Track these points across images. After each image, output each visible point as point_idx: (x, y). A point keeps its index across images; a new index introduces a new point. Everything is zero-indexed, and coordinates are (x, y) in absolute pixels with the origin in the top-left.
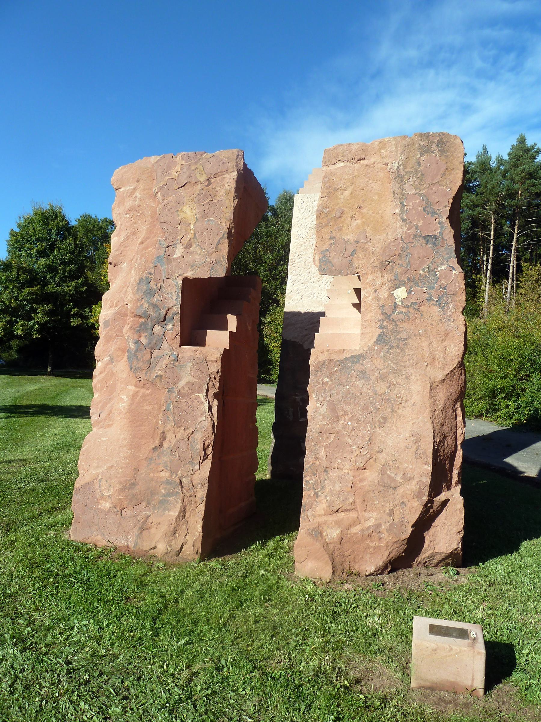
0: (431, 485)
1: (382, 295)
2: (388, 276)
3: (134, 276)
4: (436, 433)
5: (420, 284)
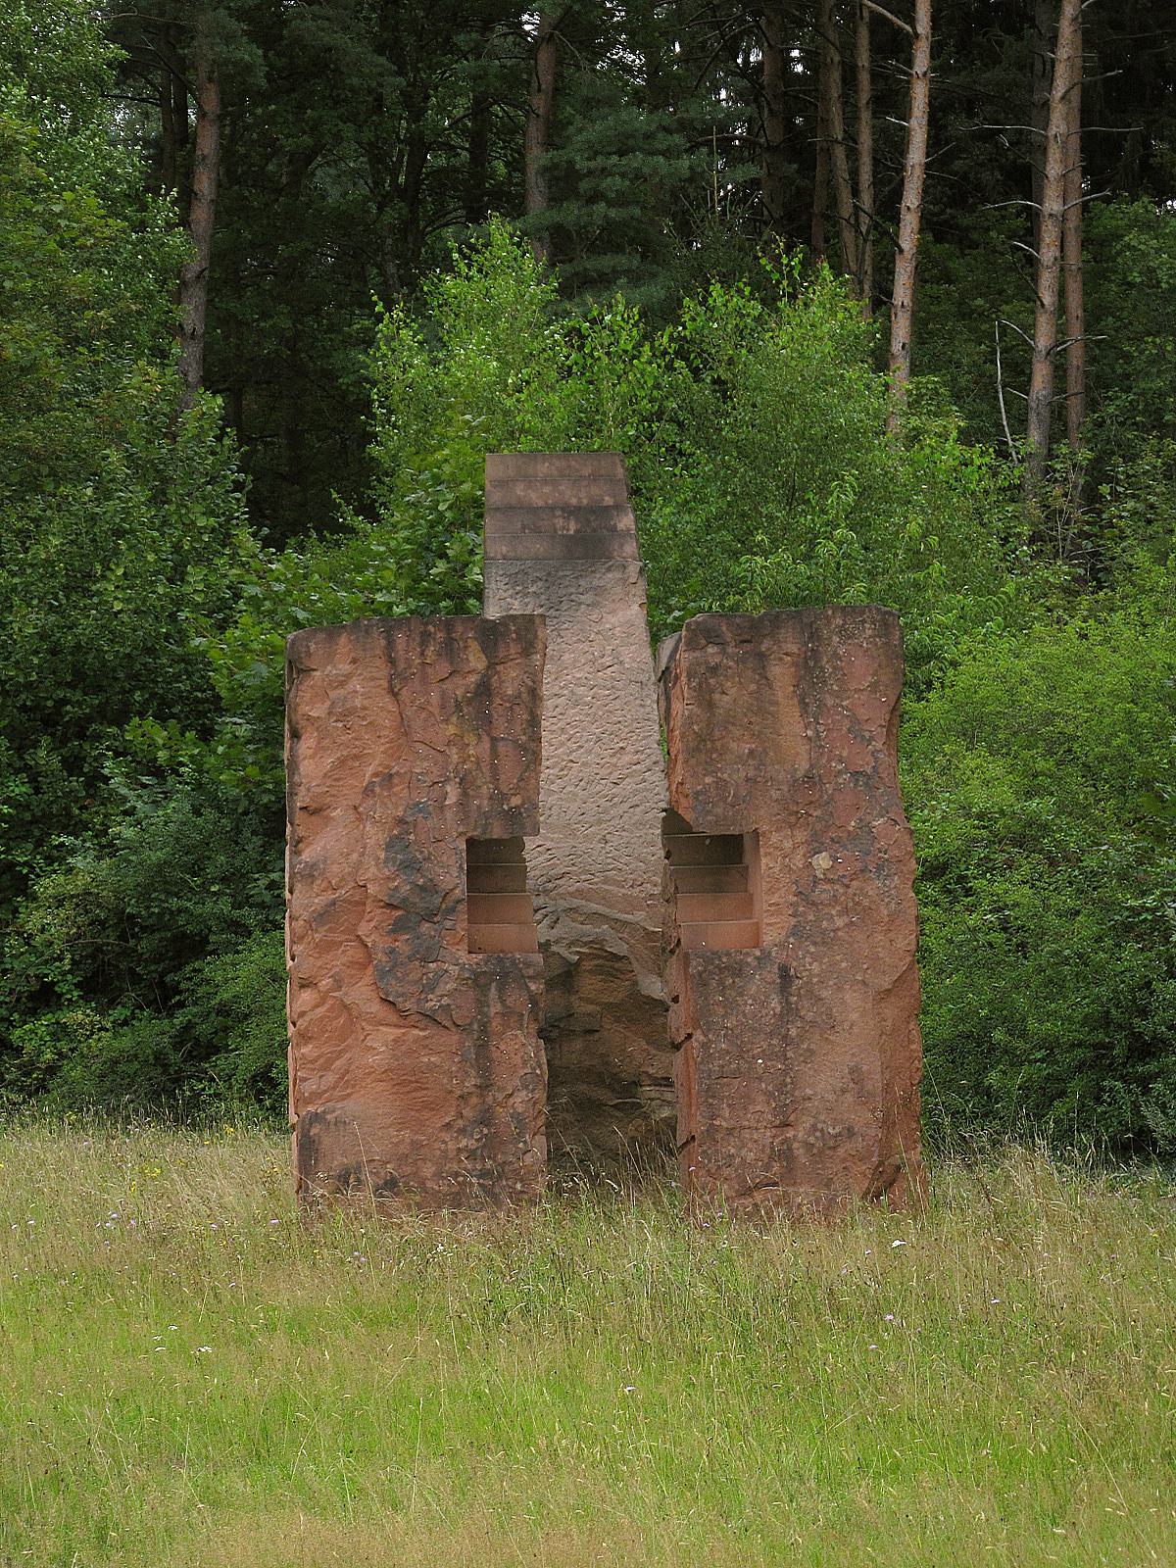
2: (801, 836)
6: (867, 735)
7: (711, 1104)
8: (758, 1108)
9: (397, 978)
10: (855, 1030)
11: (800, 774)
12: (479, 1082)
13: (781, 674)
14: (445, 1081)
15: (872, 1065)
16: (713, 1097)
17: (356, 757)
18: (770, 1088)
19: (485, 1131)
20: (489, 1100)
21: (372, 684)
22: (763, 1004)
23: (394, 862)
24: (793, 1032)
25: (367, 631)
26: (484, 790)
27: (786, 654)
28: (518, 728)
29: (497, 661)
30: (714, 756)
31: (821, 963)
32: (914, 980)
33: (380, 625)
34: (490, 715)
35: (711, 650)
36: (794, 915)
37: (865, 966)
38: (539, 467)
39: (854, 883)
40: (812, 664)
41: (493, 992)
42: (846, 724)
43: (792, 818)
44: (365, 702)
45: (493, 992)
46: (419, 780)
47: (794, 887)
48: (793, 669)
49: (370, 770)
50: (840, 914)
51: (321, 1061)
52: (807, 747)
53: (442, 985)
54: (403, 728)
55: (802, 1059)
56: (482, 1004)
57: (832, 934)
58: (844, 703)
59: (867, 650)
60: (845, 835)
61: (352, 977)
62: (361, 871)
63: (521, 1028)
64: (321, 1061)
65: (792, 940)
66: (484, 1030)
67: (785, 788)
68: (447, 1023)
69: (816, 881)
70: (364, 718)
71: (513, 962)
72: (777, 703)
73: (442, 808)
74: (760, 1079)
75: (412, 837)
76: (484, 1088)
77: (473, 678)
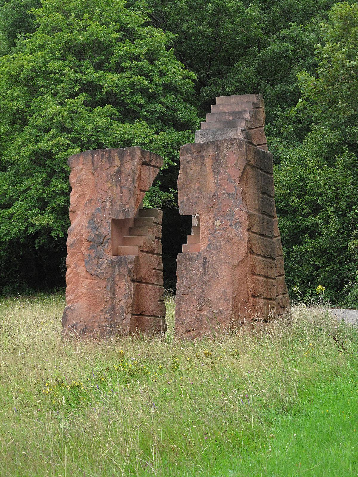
0: (65, 253)
1: (209, 224)
2: (211, 215)
3: (86, 219)
4: (234, 291)
5: (226, 218)
6: (233, 181)
10: (225, 278)
11: (212, 195)
13: (208, 161)
15: (230, 290)
17: (83, 194)
18: (197, 298)
19: (112, 312)
20: (114, 302)
21: (88, 171)
22: (198, 270)
24: (206, 279)
26: (118, 203)
28: (129, 183)
32: (248, 261)
33: (91, 153)
34: (121, 179)
35: (188, 155)
36: (209, 241)
39: (228, 230)
41: (117, 268)
42: (227, 177)
43: (210, 210)
45: (117, 268)
46: (98, 201)
48: (211, 160)
53: (102, 266)
54: (96, 185)
56: (113, 271)
63: (125, 279)
66: (113, 280)
67: (207, 199)
69: (216, 230)
71: (124, 259)
72: (206, 172)
74: (195, 295)
76: (113, 298)
77: (116, 168)
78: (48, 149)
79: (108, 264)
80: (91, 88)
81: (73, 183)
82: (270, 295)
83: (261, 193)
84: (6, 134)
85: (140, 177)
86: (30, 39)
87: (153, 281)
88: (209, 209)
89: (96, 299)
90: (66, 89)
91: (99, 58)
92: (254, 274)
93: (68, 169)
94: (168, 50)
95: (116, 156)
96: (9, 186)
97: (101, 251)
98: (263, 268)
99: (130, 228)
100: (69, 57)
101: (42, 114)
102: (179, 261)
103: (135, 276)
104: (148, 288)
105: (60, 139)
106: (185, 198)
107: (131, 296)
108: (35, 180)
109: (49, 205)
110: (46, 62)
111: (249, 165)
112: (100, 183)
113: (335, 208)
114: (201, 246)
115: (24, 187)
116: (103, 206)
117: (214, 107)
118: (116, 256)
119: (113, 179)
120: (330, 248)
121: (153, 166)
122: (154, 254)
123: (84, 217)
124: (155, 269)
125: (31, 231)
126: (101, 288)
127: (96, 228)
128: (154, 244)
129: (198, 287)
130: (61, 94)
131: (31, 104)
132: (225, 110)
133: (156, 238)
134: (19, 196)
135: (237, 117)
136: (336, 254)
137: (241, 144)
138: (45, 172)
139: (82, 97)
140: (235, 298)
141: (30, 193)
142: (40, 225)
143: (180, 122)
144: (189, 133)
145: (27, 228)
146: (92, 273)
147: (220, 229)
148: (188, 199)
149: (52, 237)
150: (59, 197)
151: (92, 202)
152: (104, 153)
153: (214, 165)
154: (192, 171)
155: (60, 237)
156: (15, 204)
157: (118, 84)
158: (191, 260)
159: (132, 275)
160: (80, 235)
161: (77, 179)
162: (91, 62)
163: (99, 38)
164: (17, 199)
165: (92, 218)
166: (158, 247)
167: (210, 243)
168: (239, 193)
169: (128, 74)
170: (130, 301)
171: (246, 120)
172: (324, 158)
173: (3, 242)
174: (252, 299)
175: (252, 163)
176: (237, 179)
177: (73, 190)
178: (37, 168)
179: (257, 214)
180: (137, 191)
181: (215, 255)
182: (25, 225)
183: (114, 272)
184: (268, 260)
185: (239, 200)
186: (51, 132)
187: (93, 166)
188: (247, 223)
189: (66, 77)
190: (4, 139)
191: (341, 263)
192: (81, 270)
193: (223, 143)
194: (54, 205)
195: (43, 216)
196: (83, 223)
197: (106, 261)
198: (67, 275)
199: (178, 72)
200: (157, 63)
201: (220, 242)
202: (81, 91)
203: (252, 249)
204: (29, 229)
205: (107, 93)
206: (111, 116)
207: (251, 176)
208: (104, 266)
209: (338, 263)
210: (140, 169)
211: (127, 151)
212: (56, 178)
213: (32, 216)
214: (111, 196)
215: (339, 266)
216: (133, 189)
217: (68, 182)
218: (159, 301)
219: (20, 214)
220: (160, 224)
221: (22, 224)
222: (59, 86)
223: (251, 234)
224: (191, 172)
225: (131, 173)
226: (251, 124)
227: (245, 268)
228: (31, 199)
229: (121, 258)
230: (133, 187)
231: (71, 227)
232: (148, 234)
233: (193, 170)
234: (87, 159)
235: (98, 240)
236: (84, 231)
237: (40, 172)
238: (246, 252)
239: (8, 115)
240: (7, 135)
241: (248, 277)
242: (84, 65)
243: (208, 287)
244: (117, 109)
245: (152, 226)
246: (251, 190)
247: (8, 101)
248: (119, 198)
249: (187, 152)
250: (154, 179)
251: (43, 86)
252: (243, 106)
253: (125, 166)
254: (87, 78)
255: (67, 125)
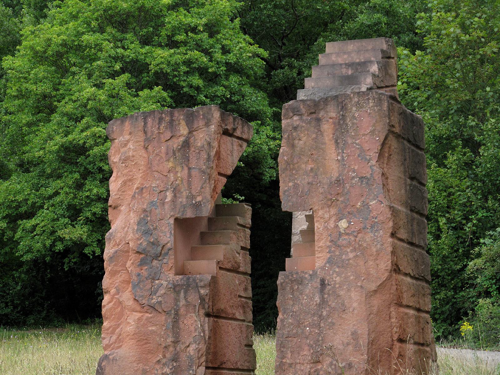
1: (330, 226)
2: (333, 211)
3: (133, 218)
5: (357, 216)
6: (368, 157)
7: (282, 351)
8: (305, 353)
9: (140, 288)
10: (356, 312)
11: (333, 179)
12: (173, 339)
13: (327, 128)
14: (158, 339)
15: (363, 330)
16: (284, 347)
17: (130, 180)
18: (312, 343)
19: (175, 364)
20: (178, 349)
21: (137, 144)
22: (312, 299)
23: (141, 231)
24: (325, 313)
25: (136, 119)
26: (184, 194)
27: (330, 118)
28: (202, 162)
29: (193, 129)
30: (294, 172)
31: (341, 277)
32: (392, 285)
33: (142, 115)
34: (189, 156)
35: (295, 118)
36: (329, 252)
37: (363, 278)
38: (349, 47)
39: (360, 235)
40: (342, 122)
41: (182, 294)
42: (358, 152)
43: (330, 203)
44: (134, 153)
45: (182, 294)
46: (154, 190)
47: (330, 238)
48: (333, 126)
49: (136, 186)
50: (351, 252)
51: (111, 329)
52: (338, 165)
53: (159, 291)
54: (149, 165)
55: (328, 327)
56: (177, 300)
57: (347, 262)
58: (357, 142)
59: (370, 114)
60: (355, 210)
61: (124, 288)
62: (127, 236)
63: (194, 312)
64: (111, 329)
65: (327, 265)
66: (177, 314)
67: (326, 187)
68: (160, 311)
69: (340, 235)
70: (133, 161)
71: (194, 280)
72: (325, 144)
73: (163, 204)
74: (307, 338)
75: (149, 218)
76: (176, 342)
77: (182, 139)
78: (81, 142)
79: (169, 288)
80: (136, 68)
81: (114, 163)
82: (423, 338)
83: (409, 178)
84: (29, 125)
85: (218, 154)
86: (60, 8)
87: (238, 316)
88: (329, 203)
89: (150, 343)
90: (104, 67)
91: (146, 30)
92: (400, 305)
93: (106, 168)
94: (232, 20)
95: (181, 121)
96: (31, 190)
97: (157, 268)
98: (413, 296)
99: (202, 233)
100: (109, 29)
101: (73, 98)
102: (282, 284)
103: (211, 307)
104: (230, 326)
105: (96, 129)
106: (291, 184)
107: (205, 339)
108: (64, 182)
109: (82, 214)
110: (79, 34)
111: (393, 132)
112: (156, 162)
113: (448, 219)
114: (317, 260)
115: (50, 191)
116: (160, 198)
117: (323, 57)
118: (181, 277)
119: (177, 155)
120: (443, 270)
121: (238, 138)
122: (238, 272)
123: (131, 214)
124: (240, 296)
125: (59, 247)
126: (158, 326)
127: (151, 233)
128: (240, 258)
129: (311, 326)
130: (97, 73)
131: (60, 87)
132: (340, 61)
133: (243, 248)
134: (44, 203)
135: (359, 70)
136: (450, 278)
137: (380, 100)
138: (77, 172)
139: (125, 77)
140: (371, 343)
141: (58, 199)
142: (71, 239)
143: (248, 114)
144: (257, 124)
145: (54, 242)
146: (144, 302)
147: (347, 234)
148: (296, 186)
149: (86, 255)
150: (95, 204)
151: (144, 191)
152: (163, 115)
153: (338, 133)
154: (301, 142)
155: (96, 254)
156: (38, 213)
157: (169, 62)
158: (300, 282)
159: (206, 306)
160: (124, 242)
161: (121, 157)
162: (135, 34)
163: (146, 5)
164: (42, 207)
165: (144, 217)
166: (245, 262)
167: (331, 256)
168: (378, 177)
169: (182, 49)
170: (203, 347)
171: (373, 74)
172: (431, 155)
173: (24, 262)
174: (397, 345)
175: (397, 130)
176: (373, 155)
177: (114, 175)
178: (66, 167)
179: (404, 210)
180: (215, 174)
181: (338, 274)
182: (51, 240)
183: (177, 302)
184: (419, 283)
185: (377, 188)
186: (84, 121)
187: (146, 136)
188: (391, 224)
189: (103, 53)
190: (26, 131)
191: (455, 289)
192: (127, 297)
193: (351, 98)
194: (89, 214)
195: (75, 227)
196: (130, 224)
197: (165, 283)
198: (105, 306)
199: (245, 49)
200: (219, 36)
201: (347, 254)
202: (123, 71)
203: (397, 266)
204: (56, 244)
205: (156, 73)
206: (161, 102)
207: (395, 150)
208: (162, 292)
209: (452, 289)
210: (220, 141)
211: (198, 111)
212: (91, 179)
213: (60, 228)
214: (174, 182)
215: (453, 293)
216: (208, 171)
217: (106, 185)
218: (246, 346)
219: (45, 226)
220: (247, 228)
221: (47, 238)
222: (95, 64)
223: (396, 241)
224: (300, 144)
225: (205, 146)
226: (380, 80)
227: (388, 296)
228: (59, 206)
229: (188, 279)
230: (208, 168)
231: (111, 231)
232: (230, 242)
233: (303, 141)
234: (136, 126)
235: (153, 251)
236: (130, 236)
237: (71, 173)
238: (389, 271)
239: (32, 102)
240: (29, 127)
241: (392, 309)
242: (128, 38)
243: (328, 325)
244: (169, 93)
245: (236, 230)
246: (396, 173)
247: (32, 84)
248: (186, 186)
249: (293, 112)
250: (239, 157)
251: (74, 65)
252: (367, 55)
253: (196, 136)
254: (130, 54)
255: (105, 112)
